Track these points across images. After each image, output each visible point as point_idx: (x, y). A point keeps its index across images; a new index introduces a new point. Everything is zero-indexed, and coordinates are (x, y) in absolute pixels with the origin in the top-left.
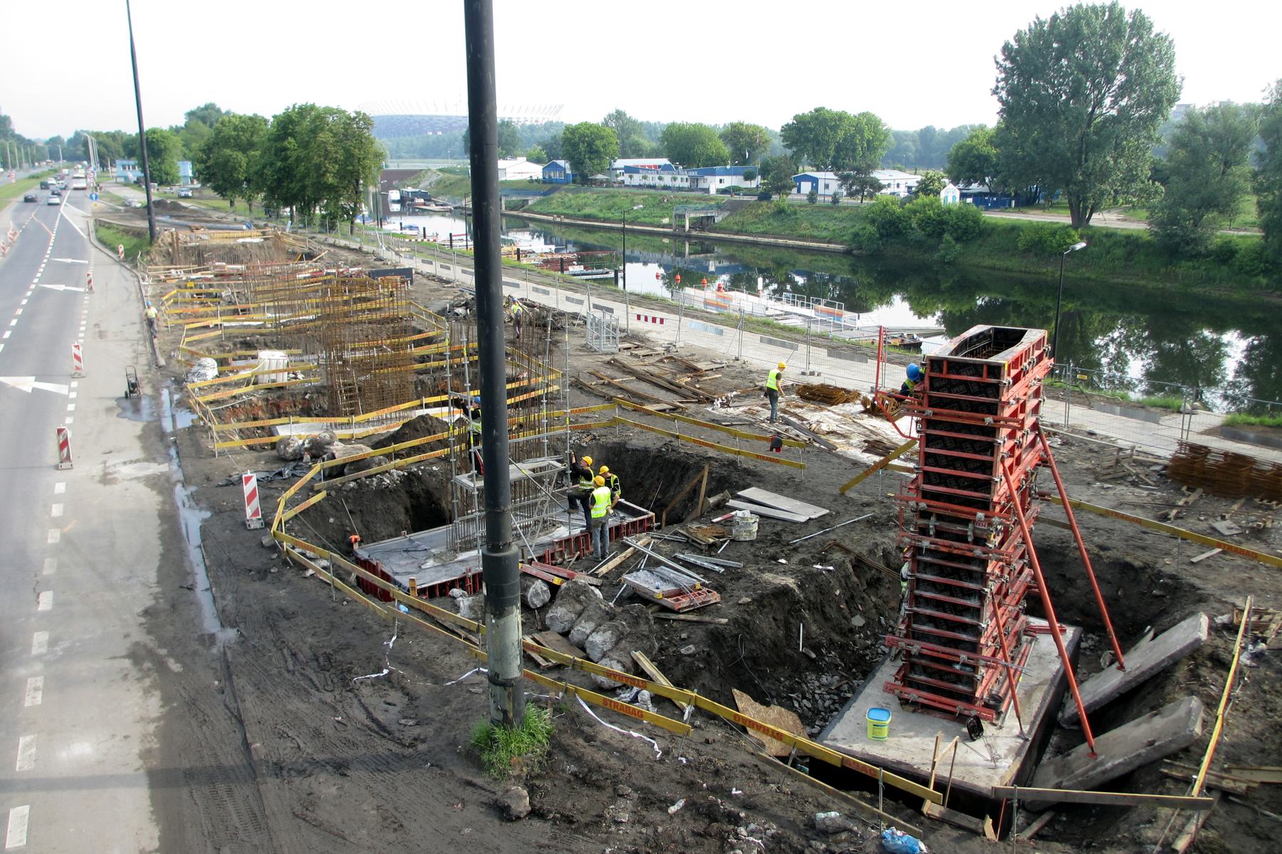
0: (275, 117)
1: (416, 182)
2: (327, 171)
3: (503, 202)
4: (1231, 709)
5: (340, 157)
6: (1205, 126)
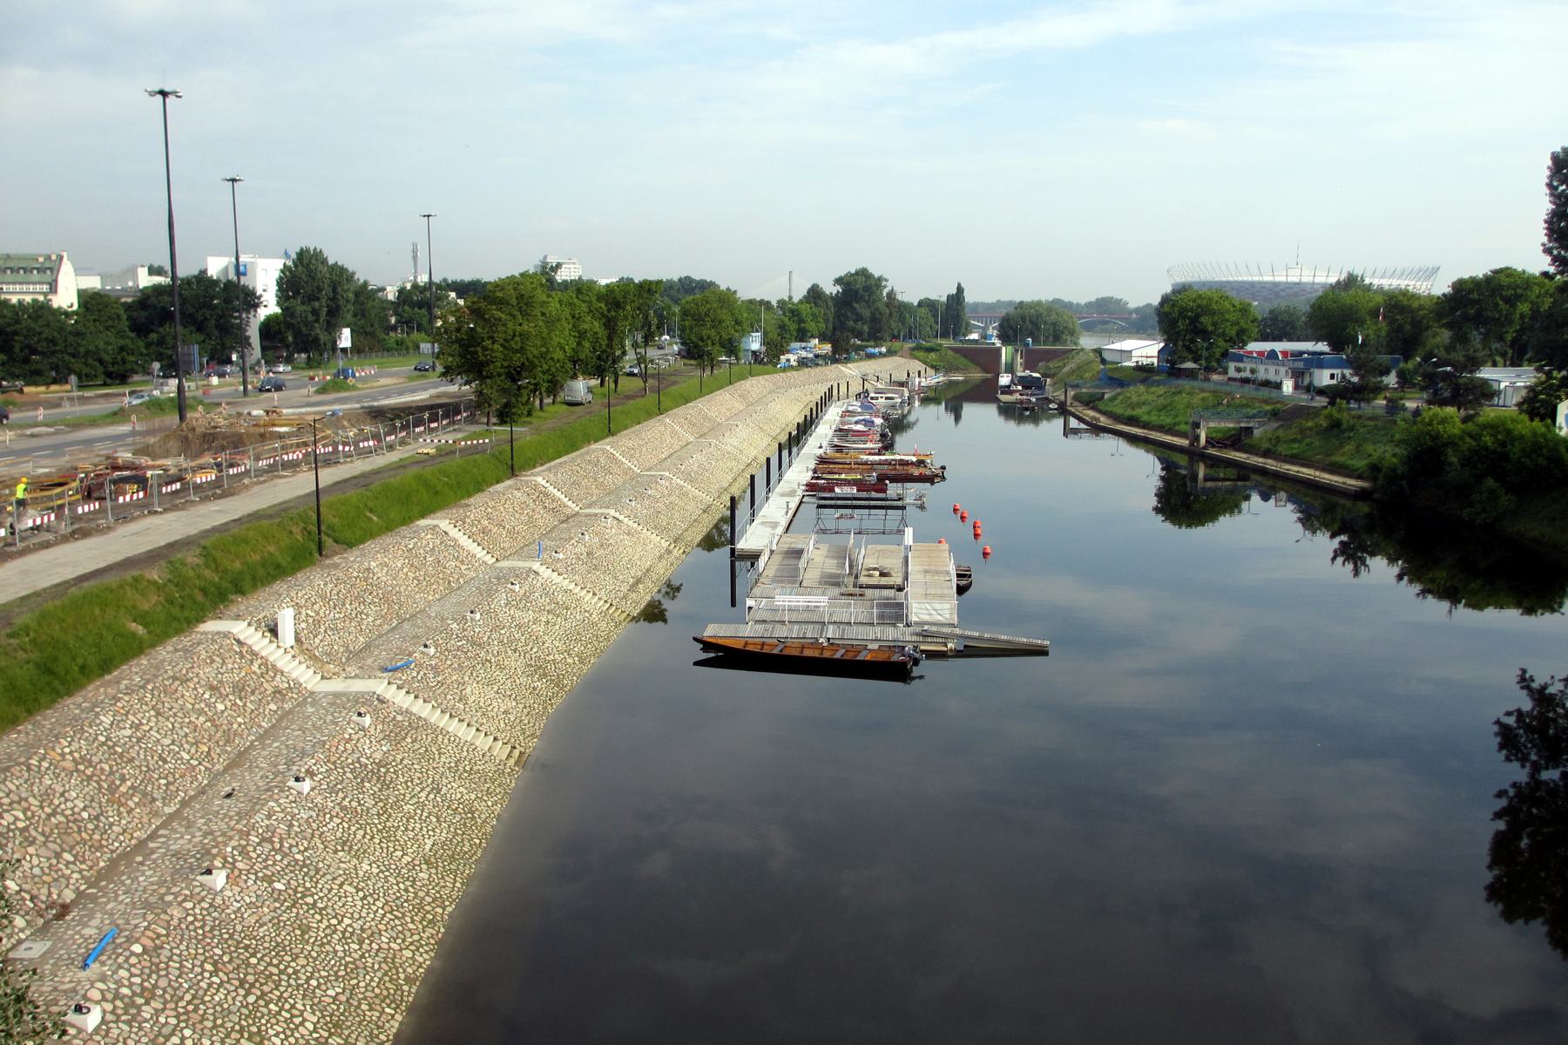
1: (1061, 364)
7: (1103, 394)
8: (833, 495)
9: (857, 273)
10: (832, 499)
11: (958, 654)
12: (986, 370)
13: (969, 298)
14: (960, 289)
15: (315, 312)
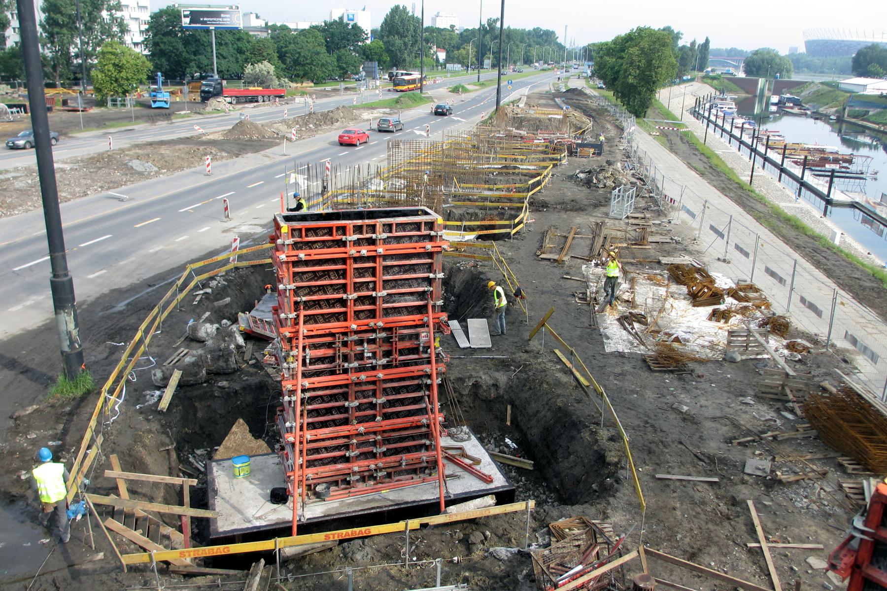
0: (509, 27)
1: (799, 90)
2: (630, 74)
3: (846, 111)
4: (862, 540)
5: (642, 65)
6: (777, 60)
7: (868, 112)
8: (823, 169)
9: (664, 30)
10: (824, 171)
11: (577, 258)
12: (747, 92)
13: (712, 46)
14: (707, 41)
15: (405, 44)
